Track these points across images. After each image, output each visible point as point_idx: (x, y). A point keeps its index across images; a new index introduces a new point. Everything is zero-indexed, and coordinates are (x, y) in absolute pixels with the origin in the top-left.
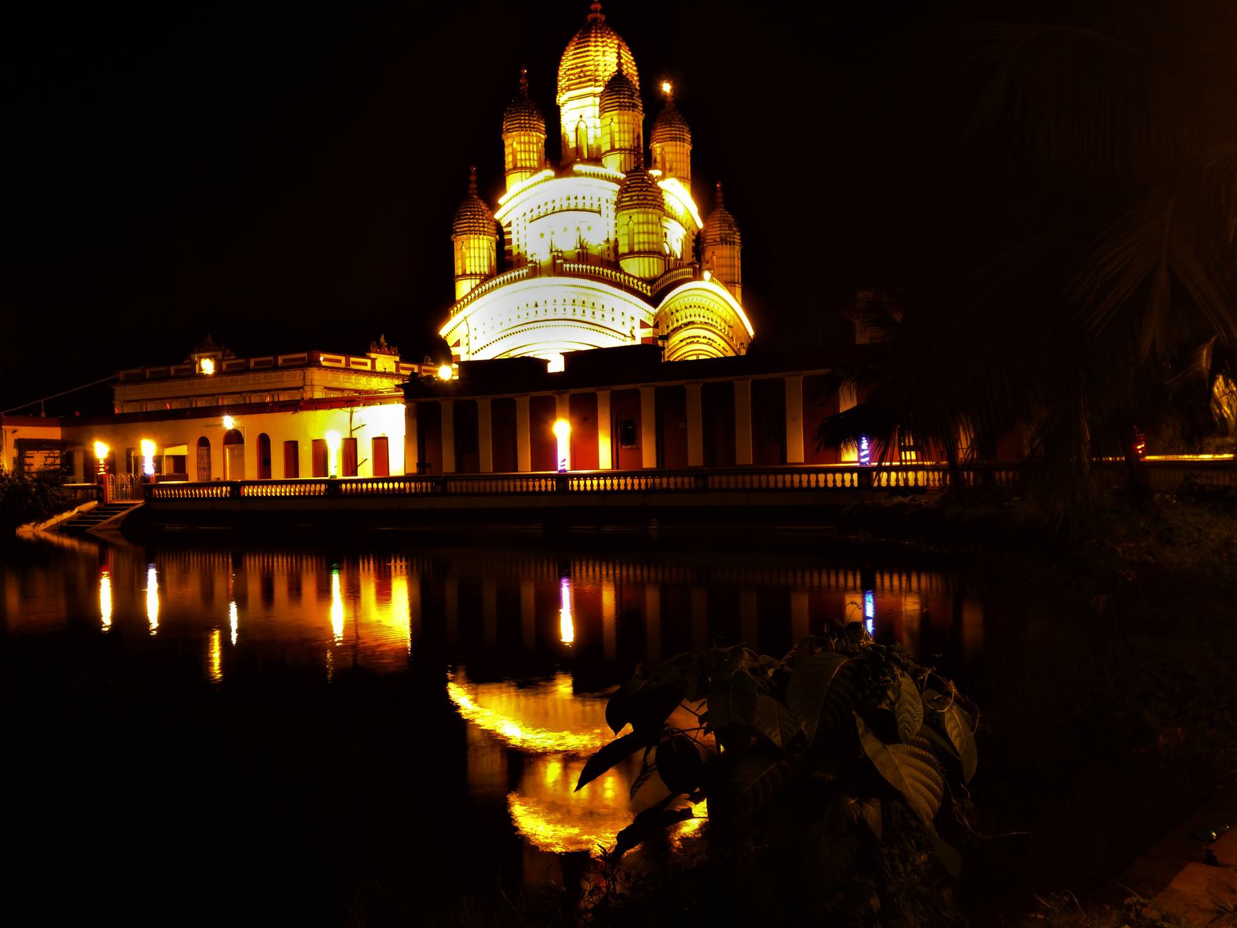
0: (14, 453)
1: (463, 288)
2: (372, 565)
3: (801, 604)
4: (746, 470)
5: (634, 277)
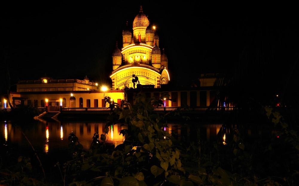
0: (12, 100)
1: (115, 68)
2: (102, 124)
3: (208, 131)
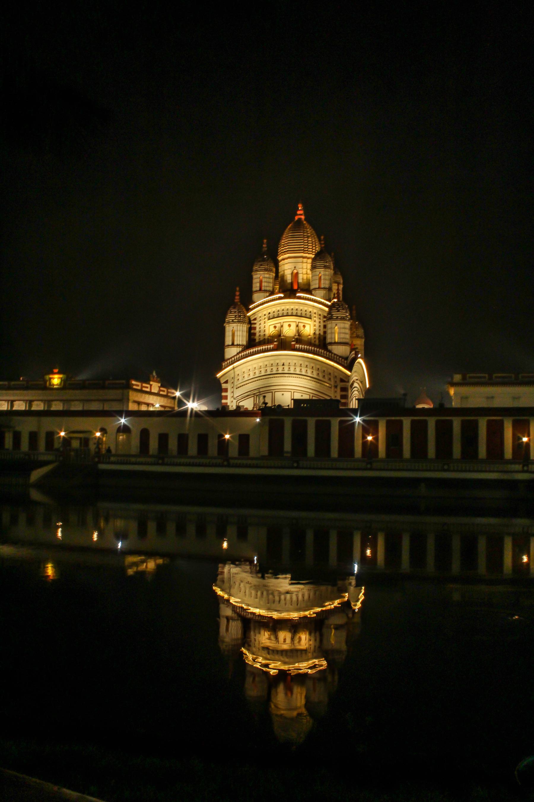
1: (231, 352)
4: (334, 460)
5: (337, 355)
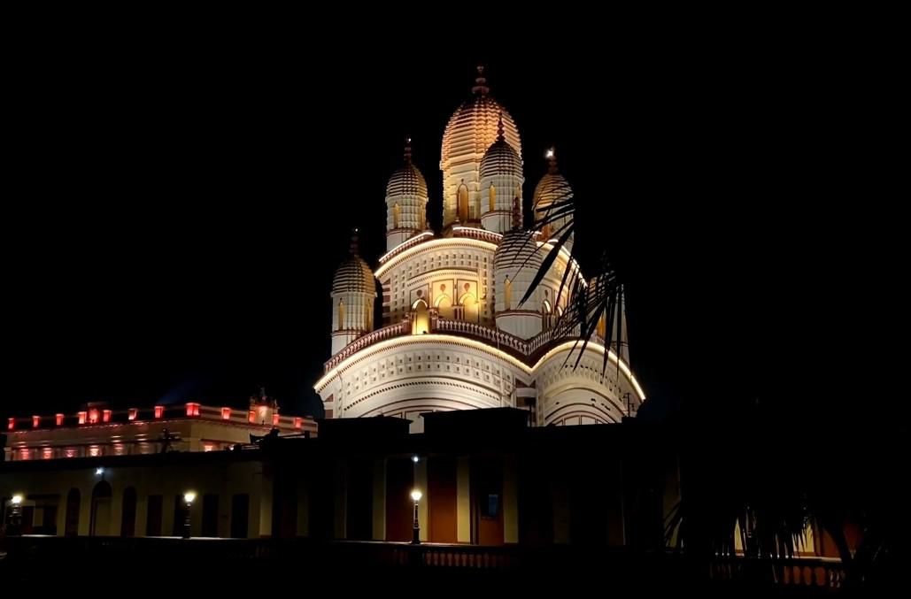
1: (339, 343)
